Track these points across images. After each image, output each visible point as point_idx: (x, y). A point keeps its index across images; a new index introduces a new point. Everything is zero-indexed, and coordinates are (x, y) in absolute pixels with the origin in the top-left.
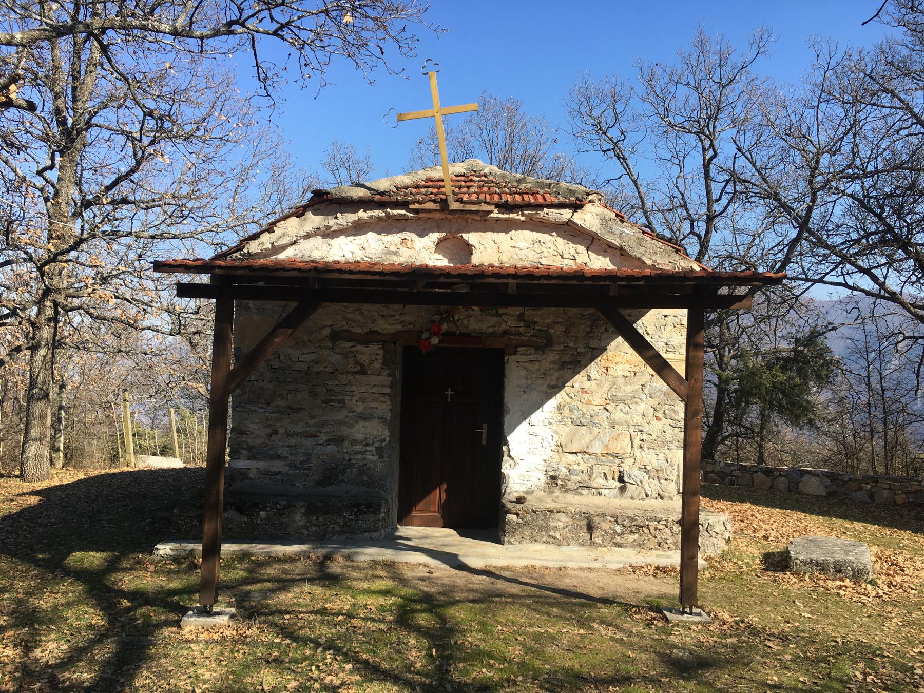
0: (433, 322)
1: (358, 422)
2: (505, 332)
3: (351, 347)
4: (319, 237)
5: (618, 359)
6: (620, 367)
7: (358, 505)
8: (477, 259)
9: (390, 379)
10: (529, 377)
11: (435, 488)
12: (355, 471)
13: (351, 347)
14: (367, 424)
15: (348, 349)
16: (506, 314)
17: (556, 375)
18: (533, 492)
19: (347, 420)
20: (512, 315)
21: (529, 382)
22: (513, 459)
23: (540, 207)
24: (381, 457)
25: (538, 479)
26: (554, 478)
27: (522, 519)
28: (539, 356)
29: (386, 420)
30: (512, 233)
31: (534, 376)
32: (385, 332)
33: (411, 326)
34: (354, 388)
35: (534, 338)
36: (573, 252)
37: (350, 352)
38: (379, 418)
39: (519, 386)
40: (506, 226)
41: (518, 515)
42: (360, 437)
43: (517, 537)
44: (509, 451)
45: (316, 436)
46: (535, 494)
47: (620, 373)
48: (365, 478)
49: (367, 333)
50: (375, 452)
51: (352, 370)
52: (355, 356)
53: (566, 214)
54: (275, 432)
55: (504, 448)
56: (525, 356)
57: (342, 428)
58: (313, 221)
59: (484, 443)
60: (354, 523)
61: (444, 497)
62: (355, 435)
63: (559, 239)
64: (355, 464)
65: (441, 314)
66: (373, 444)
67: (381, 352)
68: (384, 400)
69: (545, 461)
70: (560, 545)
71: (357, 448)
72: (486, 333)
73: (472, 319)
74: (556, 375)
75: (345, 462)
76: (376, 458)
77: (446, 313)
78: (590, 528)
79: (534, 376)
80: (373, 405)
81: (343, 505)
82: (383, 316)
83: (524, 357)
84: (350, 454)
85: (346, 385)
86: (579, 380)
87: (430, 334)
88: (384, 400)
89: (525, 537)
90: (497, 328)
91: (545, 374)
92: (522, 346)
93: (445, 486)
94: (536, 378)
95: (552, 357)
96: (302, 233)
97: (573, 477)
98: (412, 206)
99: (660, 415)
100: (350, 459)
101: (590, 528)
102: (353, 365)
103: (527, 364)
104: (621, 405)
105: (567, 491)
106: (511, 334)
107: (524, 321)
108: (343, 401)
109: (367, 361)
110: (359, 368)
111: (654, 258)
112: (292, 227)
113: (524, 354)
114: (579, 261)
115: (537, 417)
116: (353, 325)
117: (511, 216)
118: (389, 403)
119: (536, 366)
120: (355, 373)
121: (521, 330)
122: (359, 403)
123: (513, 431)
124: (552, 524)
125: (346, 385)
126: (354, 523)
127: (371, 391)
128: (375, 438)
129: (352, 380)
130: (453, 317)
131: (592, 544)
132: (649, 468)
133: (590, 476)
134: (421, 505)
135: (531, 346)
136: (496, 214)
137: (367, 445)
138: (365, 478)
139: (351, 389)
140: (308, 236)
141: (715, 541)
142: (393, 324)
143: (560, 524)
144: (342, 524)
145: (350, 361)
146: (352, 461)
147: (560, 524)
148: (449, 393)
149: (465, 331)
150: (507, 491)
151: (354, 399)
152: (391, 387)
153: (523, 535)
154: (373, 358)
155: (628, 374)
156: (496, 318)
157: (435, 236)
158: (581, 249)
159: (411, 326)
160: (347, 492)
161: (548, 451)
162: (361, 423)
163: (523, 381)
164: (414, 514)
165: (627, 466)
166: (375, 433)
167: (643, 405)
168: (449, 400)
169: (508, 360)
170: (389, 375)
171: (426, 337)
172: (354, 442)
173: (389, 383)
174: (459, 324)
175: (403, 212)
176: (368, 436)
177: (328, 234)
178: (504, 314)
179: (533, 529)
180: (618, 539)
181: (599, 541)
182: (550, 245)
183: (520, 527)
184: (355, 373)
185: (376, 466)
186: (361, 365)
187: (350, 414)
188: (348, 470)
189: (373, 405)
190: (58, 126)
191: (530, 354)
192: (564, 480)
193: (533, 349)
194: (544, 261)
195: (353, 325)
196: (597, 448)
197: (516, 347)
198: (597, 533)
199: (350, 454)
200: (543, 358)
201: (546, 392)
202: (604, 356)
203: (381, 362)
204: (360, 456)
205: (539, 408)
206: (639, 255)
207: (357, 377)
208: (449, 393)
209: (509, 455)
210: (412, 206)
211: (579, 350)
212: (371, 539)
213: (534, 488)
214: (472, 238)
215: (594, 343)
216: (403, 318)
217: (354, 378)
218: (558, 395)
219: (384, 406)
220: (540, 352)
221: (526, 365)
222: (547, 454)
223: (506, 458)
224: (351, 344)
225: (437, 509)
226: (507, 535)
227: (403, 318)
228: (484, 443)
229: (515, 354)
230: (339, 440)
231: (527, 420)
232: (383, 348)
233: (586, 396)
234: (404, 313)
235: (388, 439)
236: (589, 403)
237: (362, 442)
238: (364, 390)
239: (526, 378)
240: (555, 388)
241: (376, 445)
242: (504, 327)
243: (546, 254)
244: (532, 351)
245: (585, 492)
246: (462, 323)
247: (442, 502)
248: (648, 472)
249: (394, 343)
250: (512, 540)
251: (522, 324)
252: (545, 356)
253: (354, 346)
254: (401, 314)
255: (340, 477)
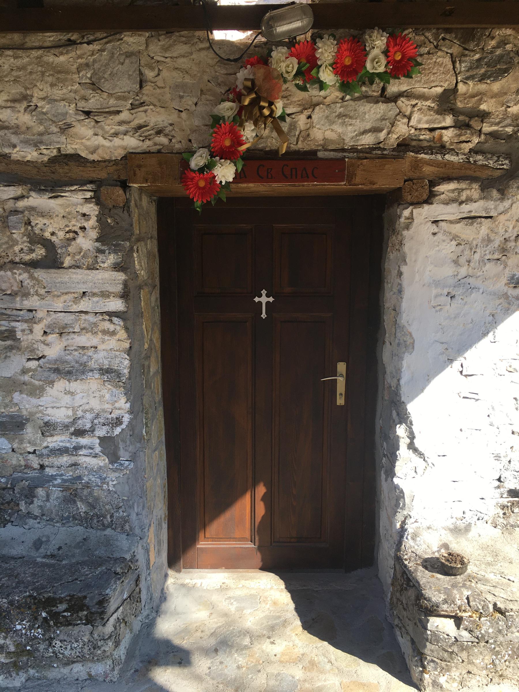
0: (217, 120)
1: (52, 383)
3: (17, 199)
7: (50, 602)
9: (121, 276)
10: (462, 260)
11: (242, 493)
12: (56, 493)
13: (17, 199)
14: (74, 386)
15: (10, 205)
18: (468, 528)
19: (26, 378)
20: (423, 97)
22: (421, 455)
24: (114, 458)
27: (470, 631)
28: (491, 204)
29: (119, 375)
31: (477, 257)
32: (91, 157)
33: (163, 140)
34: (32, 302)
35: (480, 157)
37: (15, 212)
38: (105, 371)
39: (437, 283)
41: (458, 621)
43: (455, 673)
44: (412, 436)
46: (473, 534)
48: (82, 507)
49: (53, 160)
50: (98, 449)
51: (27, 258)
52: (29, 223)
55: (401, 431)
56: (455, 205)
57: (17, 397)
59: (340, 401)
60: (42, 647)
61: (261, 510)
62: (50, 411)
64: (53, 478)
65: (238, 97)
66: (92, 430)
67: (92, 209)
68: (112, 327)
69: (498, 457)
72: (353, 150)
73: (318, 114)
75: (32, 474)
76: (102, 461)
77: (250, 90)
79: (477, 257)
80: (83, 340)
81: (11, 603)
82: (88, 113)
83: (453, 208)
84: (41, 456)
85: (13, 295)
87: (212, 156)
88: (112, 327)
89: (474, 670)
90: (382, 135)
91: (504, 250)
92: (449, 179)
93: (261, 490)
94: (482, 262)
100: (42, 467)
102: (25, 246)
103: (458, 226)
106: (419, 149)
107: (453, 111)
109: (61, 234)
110: (40, 252)
113: (454, 200)
116: (14, 139)
118: (122, 334)
120: (34, 264)
121: (448, 135)
122: (51, 338)
123: (422, 390)
125: (13, 295)
126: (42, 647)
127: (75, 308)
128: (97, 416)
129: (27, 282)
130: (271, 104)
134: (214, 528)
135: (473, 179)
137: (80, 433)
138: (82, 507)
139: (28, 303)
142: (116, 134)
144: (12, 649)
145: (17, 234)
146: (49, 471)
148: (264, 299)
149: (301, 146)
150: (410, 528)
151: (38, 329)
152: (125, 295)
153: (470, 668)
154: (75, 224)
156: (382, 108)
159: (163, 140)
160: (38, 544)
162: (61, 385)
163: (448, 271)
164: (202, 544)
166: (96, 404)
168: (264, 315)
169: (411, 218)
170: (117, 267)
171: (202, 163)
173: (119, 288)
174: (285, 127)
176: (80, 413)
178: (401, 95)
179: (497, 653)
183: (463, 648)
184: (34, 264)
185: (103, 480)
186: (48, 245)
187: (33, 364)
188: (40, 492)
189: (83, 340)
190: (32, 96)
191: (469, 200)
193: (476, 186)
195: (14, 139)
197: (433, 184)
199: (41, 456)
200: (501, 208)
201: (506, 296)
203: (94, 234)
204: (65, 460)
205: (485, 334)
207: (40, 274)
208: (264, 299)
209: (411, 446)
212: (90, 677)
213: (470, 517)
216: (140, 118)
217: (32, 277)
219: (112, 343)
220: (495, 193)
221: (458, 228)
223: (403, 451)
224: (18, 191)
225: (247, 534)
226: (430, 667)
227: (140, 118)
228: (340, 401)
229: (428, 201)
231: (456, 365)
232: (97, 199)
234: (142, 104)
235: (126, 419)
237: (66, 427)
238: (59, 305)
239: (456, 262)
241: (101, 432)
244: (474, 191)
246: (293, 126)
247: (258, 519)
249: (124, 185)
250: (442, 680)
251: (449, 120)
252: (507, 204)
253: (22, 197)
254: (133, 107)
255: (23, 506)
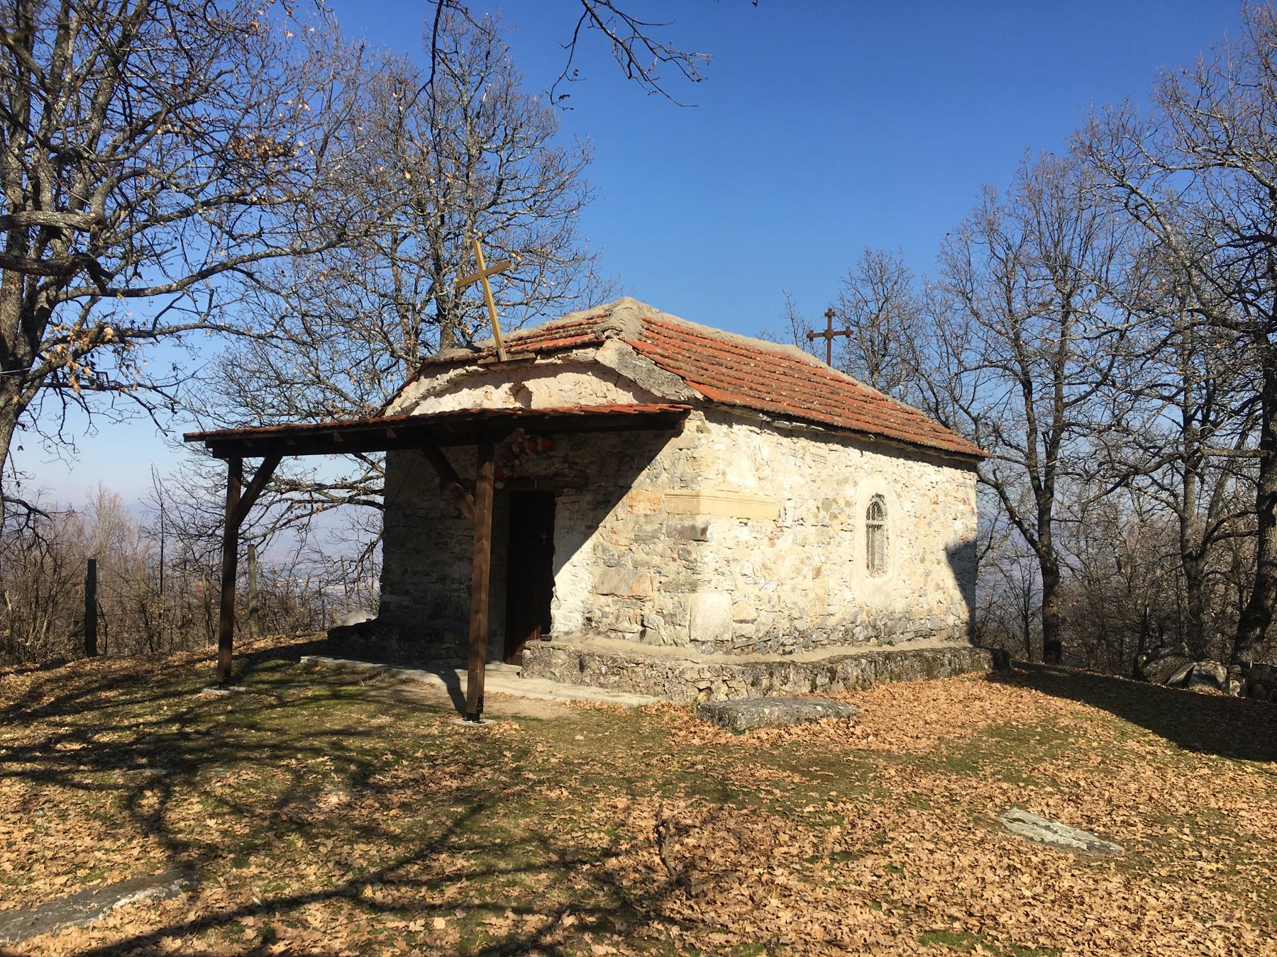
2: (556, 474)
4: (715, 400)
5: (641, 497)
6: (642, 505)
8: (537, 404)
16: (555, 457)
17: (592, 515)
21: (572, 523)
23: (568, 349)
25: (578, 620)
26: (589, 619)
30: (559, 376)
36: (604, 389)
40: (553, 371)
42: (457, 576)
45: (430, 575)
47: (642, 512)
53: (590, 353)
54: (406, 570)
58: (425, 383)
63: (594, 378)
70: (559, 681)
71: (455, 586)
74: (592, 515)
78: (582, 667)
86: (609, 520)
95: (589, 497)
96: (419, 395)
97: (604, 620)
98: (480, 362)
99: (676, 556)
101: (582, 667)
104: (643, 546)
105: (599, 633)
108: (446, 544)
111: (661, 389)
112: (412, 392)
114: (609, 398)
115: (577, 558)
117: (550, 360)
119: (576, 507)
124: (554, 661)
131: (582, 682)
132: (665, 612)
133: (617, 619)
136: (539, 361)
137: (461, 583)
140: (424, 397)
141: (685, 688)
143: (560, 661)
147: (560, 661)
155: (649, 512)
157: (506, 386)
158: (611, 386)
161: (586, 592)
163: (567, 523)
165: (648, 610)
167: (661, 545)
172: (453, 581)
175: (476, 368)
177: (439, 394)
180: (602, 680)
181: (588, 680)
182: (587, 385)
192: (597, 622)
194: (583, 402)
196: (624, 591)
198: (588, 672)
202: (629, 494)
204: (457, 594)
206: (648, 388)
210: (480, 362)
211: (609, 489)
213: (574, 629)
214: (531, 384)
215: (621, 483)
218: (594, 536)
222: (584, 595)
230: (442, 579)
233: (614, 536)
236: (617, 543)
240: (592, 528)
242: (553, 469)
243: (584, 394)
245: (613, 635)
248: (664, 617)
